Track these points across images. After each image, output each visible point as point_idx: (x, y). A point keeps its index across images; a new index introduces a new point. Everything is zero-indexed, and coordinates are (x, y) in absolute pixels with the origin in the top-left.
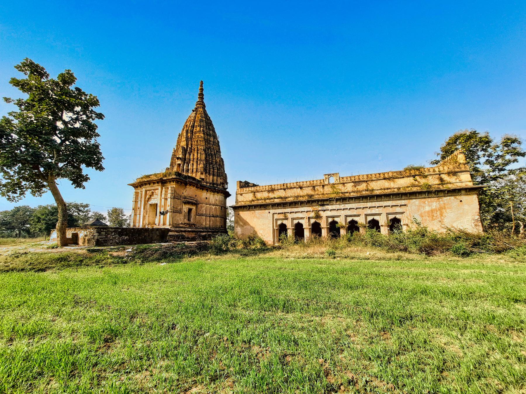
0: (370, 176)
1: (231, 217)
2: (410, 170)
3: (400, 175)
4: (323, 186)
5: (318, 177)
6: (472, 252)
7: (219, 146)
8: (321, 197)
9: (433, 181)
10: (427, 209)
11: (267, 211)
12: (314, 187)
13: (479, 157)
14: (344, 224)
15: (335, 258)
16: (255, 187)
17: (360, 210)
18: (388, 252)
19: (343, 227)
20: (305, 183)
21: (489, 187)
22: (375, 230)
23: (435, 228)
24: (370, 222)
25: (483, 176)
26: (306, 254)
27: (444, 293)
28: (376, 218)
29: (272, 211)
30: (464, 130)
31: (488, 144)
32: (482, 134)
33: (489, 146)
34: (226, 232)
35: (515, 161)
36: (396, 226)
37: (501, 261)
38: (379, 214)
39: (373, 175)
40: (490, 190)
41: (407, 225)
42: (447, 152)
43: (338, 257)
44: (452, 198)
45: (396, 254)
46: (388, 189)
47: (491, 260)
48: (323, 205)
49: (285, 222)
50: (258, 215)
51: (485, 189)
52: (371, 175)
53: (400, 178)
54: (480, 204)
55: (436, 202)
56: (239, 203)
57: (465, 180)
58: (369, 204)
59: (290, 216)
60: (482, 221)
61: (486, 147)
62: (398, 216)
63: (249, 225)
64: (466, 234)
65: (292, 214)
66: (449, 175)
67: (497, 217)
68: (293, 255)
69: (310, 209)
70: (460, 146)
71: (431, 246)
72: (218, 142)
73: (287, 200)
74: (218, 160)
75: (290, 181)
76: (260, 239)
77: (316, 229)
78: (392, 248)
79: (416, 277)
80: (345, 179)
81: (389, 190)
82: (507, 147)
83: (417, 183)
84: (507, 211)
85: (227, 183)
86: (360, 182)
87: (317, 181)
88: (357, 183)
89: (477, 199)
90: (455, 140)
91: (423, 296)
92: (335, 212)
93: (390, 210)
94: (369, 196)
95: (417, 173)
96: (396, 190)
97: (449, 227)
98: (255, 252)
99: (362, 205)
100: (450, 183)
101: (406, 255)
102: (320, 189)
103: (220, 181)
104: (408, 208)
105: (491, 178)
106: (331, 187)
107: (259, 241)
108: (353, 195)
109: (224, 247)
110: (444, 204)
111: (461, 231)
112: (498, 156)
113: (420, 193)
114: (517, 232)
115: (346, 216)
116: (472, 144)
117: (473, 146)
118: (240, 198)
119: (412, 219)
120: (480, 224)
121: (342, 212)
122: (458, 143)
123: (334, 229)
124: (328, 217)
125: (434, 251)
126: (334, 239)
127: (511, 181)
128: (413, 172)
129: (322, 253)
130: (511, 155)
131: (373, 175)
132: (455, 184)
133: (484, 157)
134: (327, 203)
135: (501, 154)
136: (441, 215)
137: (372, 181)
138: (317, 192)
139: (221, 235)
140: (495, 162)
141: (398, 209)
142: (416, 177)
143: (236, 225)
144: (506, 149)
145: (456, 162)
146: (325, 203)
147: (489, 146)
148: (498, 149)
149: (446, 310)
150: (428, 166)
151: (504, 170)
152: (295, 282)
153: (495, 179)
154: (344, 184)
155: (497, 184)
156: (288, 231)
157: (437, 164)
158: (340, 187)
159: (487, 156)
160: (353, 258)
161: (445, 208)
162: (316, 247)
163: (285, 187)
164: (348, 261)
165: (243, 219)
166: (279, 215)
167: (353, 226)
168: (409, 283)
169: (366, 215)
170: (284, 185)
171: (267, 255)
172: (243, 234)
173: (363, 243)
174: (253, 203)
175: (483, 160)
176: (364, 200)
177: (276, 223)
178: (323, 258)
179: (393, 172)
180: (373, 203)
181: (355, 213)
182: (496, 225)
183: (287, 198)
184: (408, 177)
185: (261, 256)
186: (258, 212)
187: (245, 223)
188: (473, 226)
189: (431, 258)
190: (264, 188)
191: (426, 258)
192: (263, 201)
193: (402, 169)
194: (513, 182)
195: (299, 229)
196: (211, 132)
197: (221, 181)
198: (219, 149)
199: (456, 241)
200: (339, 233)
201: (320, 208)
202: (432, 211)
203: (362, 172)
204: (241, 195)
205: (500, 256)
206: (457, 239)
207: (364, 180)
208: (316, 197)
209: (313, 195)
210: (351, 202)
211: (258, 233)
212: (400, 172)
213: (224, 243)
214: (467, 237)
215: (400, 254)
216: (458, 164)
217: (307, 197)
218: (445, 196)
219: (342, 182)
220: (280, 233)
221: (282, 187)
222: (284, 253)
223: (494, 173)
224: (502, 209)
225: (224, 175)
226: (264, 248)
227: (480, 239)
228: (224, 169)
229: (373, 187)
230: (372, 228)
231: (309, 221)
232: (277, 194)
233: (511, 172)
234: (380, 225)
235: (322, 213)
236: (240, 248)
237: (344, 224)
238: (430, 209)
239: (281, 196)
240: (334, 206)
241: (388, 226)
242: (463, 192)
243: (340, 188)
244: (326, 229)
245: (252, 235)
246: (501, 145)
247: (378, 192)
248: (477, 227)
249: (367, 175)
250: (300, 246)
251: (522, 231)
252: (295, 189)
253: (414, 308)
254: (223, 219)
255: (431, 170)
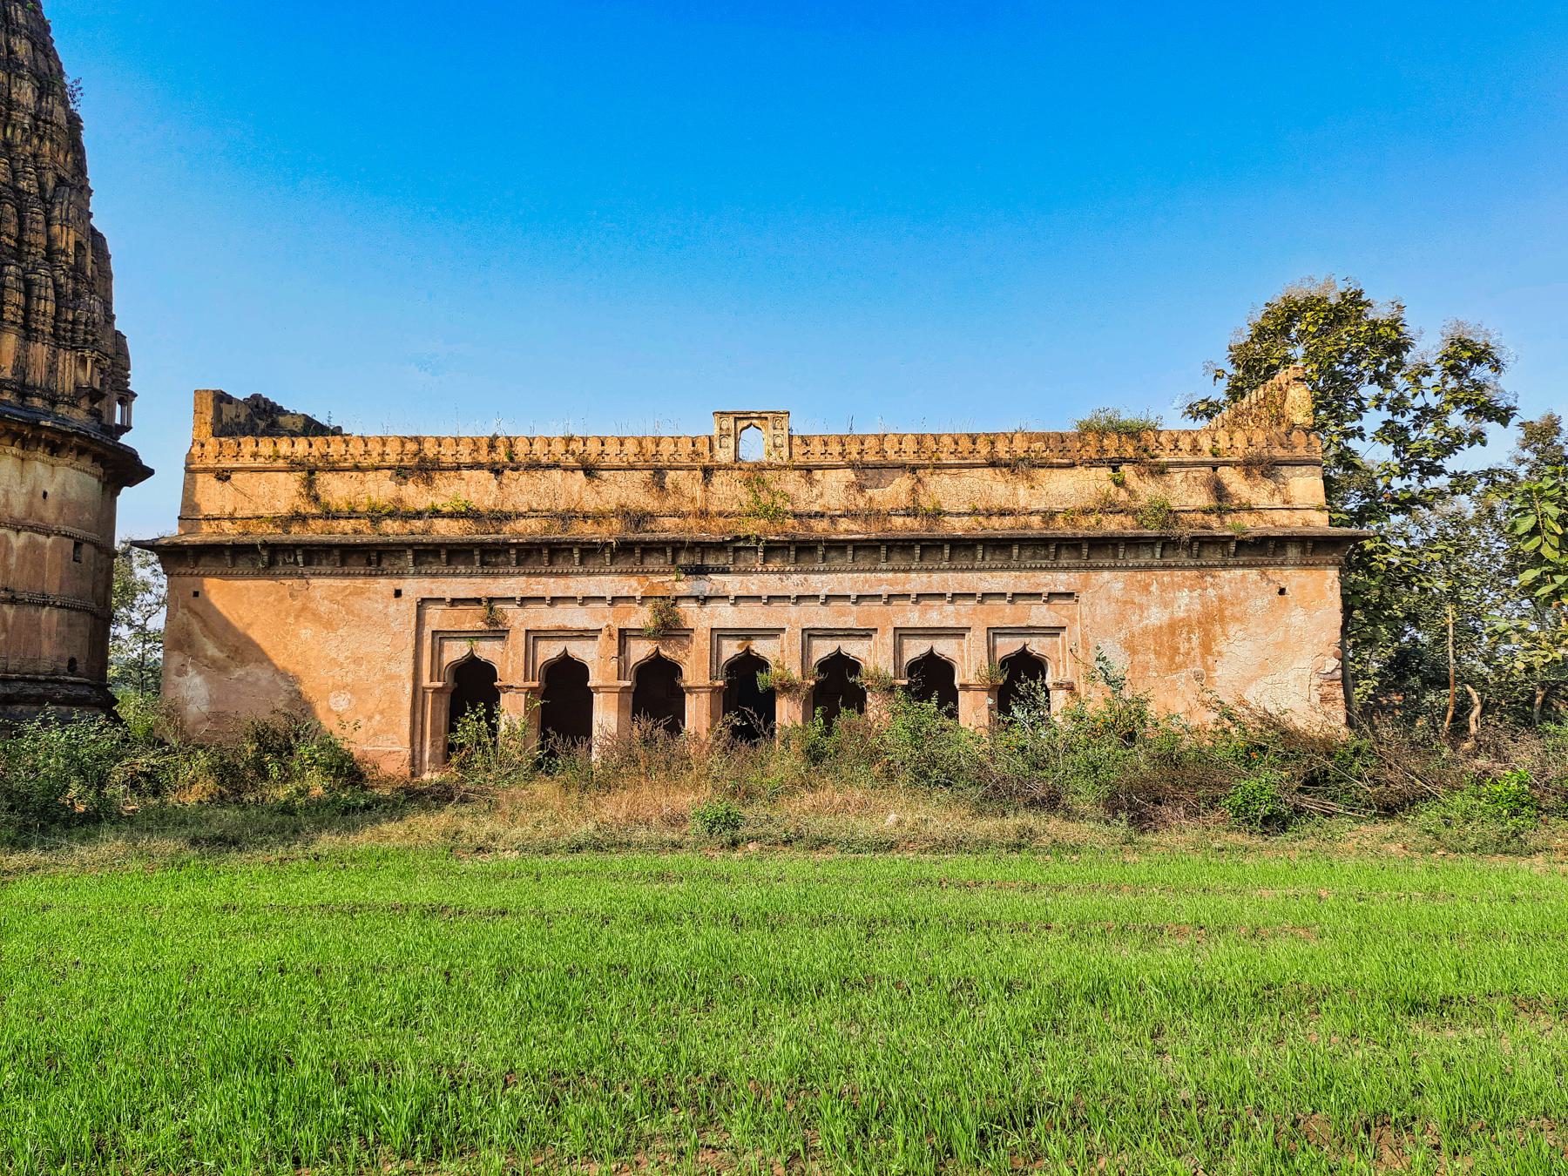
0: (930, 443)
1: (146, 611)
2: (1102, 433)
3: (1058, 453)
4: (708, 472)
5: (684, 421)
6: (1298, 811)
7: (77, 148)
8: (693, 530)
9: (1186, 494)
10: (1156, 616)
11: (384, 585)
12: (659, 472)
13: (1362, 408)
14: (796, 673)
15: (734, 844)
16: (318, 442)
17: (876, 606)
18: (981, 813)
19: (788, 688)
20: (612, 448)
21: (1384, 539)
22: (932, 706)
23: (1177, 705)
24: (914, 666)
25: (1370, 492)
26: (591, 826)
27: (1172, 995)
28: (945, 648)
29: (415, 587)
30: (1320, 279)
31: (1398, 354)
32: (1380, 312)
33: (1399, 366)
34: (107, 704)
35: (1478, 438)
36: (1022, 689)
37: (1393, 848)
38: (958, 633)
39: (947, 441)
40: (1386, 551)
41: (1071, 688)
42: (1253, 368)
43: (750, 839)
44: (1253, 574)
45: (1012, 822)
46: (1002, 513)
47: (1360, 837)
48: (700, 571)
49: (487, 651)
50: (324, 607)
51: (1369, 546)
52: (937, 439)
53: (1060, 466)
54: (1347, 610)
55: (1191, 589)
56: (206, 528)
57: (1301, 500)
58: (917, 582)
59: (519, 619)
60: (1348, 680)
61: (1388, 365)
62: (1036, 646)
63: (262, 658)
64: (1288, 735)
65: (532, 609)
66: (1248, 475)
67: (1402, 665)
68: (517, 832)
69: (630, 585)
70: (1299, 351)
71: (1157, 784)
72: (74, 122)
73: (508, 531)
74: (67, 239)
75: (537, 423)
76: (329, 746)
77: (656, 691)
78: (997, 795)
79: (1079, 930)
80: (817, 447)
81: (1008, 521)
82: (1458, 377)
83: (1123, 495)
84: (1436, 642)
85: (126, 398)
86: (885, 468)
87: (676, 440)
88: (869, 470)
89: (1337, 585)
90: (1283, 321)
91: (1094, 1014)
92: (757, 607)
93: (1006, 615)
94: (918, 541)
95: (1130, 451)
96: (1036, 520)
97: (1228, 701)
98: (289, 823)
99: (884, 581)
100: (1250, 509)
101: (1051, 826)
102: (689, 483)
103: (72, 373)
104: (1082, 609)
105: (1394, 501)
106: (748, 483)
107: (324, 757)
108: (847, 529)
109: (77, 797)
110: (1221, 599)
111: (1268, 721)
112: (1426, 411)
113: (1135, 543)
114: (1459, 729)
115: (810, 634)
116: (1341, 343)
117: (1346, 357)
118: (214, 498)
119: (1091, 661)
120: (1340, 693)
121: (793, 611)
122: (1293, 333)
123: (745, 691)
124: (719, 634)
125: (1165, 810)
126: (744, 746)
127: (1457, 521)
128: (1111, 443)
129: (676, 820)
130: (1466, 412)
131: (947, 441)
132: (1268, 515)
133: (1378, 407)
134: (722, 561)
135: (1434, 402)
136: (1206, 648)
137: (939, 467)
138: (671, 502)
139: (64, 721)
140: (1413, 435)
141: (1039, 614)
142: (1123, 468)
143: (177, 659)
144: (1452, 383)
145: (1279, 419)
146: (710, 561)
147: (1399, 366)
148: (1426, 381)
149: (1174, 1066)
150: (1174, 421)
151: (1439, 471)
152: (503, 979)
153: (1405, 505)
154: (809, 470)
155: (1412, 530)
156: (505, 700)
157: (1210, 416)
158: (792, 483)
159: (1390, 408)
160: (820, 844)
161: (1222, 619)
162: (646, 790)
163: (501, 455)
164: (795, 863)
165: (227, 625)
166: (456, 612)
167: (837, 685)
168: (1050, 958)
169: (902, 634)
170: (492, 447)
171: (364, 840)
172: (217, 717)
173: (877, 768)
174: (297, 533)
175: (1373, 420)
176: (898, 560)
177: (437, 653)
178: (676, 846)
179: (1031, 437)
180: (936, 577)
181: (850, 622)
182: (1397, 699)
183: (507, 517)
184: (1092, 464)
185: (326, 842)
186: (324, 588)
187: (242, 649)
188: (1316, 699)
189: (1149, 838)
190: (376, 449)
191: (1130, 841)
192: (364, 525)
193: (1069, 428)
194: (1465, 527)
195: (563, 694)
196: (22, 47)
197: (84, 377)
198: (80, 168)
199: (1248, 763)
200: (771, 715)
201: (685, 586)
202: (1173, 627)
203: (892, 419)
204: (223, 476)
205: (1388, 829)
206: (1253, 752)
207: (905, 458)
208: (669, 528)
209: (652, 516)
210: (838, 562)
211: (320, 710)
212: (1062, 438)
213: (81, 772)
214: (1275, 742)
215: (1030, 819)
216: (1283, 429)
217: (616, 524)
218: (1225, 566)
219: (799, 459)
220: (455, 713)
221: (483, 457)
222: (466, 825)
223: (1406, 481)
224: (1420, 636)
225: (107, 344)
226: (355, 794)
227: (1330, 755)
228: (107, 304)
229: (939, 497)
230: (923, 695)
231: (622, 648)
232: (449, 492)
233: (1462, 483)
234: (957, 682)
235: (690, 613)
236: (191, 800)
237: (796, 673)
238: (1165, 618)
239: (474, 505)
240: (754, 578)
241: (990, 690)
242: (1293, 553)
243: (790, 488)
244: (705, 697)
245: (280, 724)
246: (1439, 367)
247: (957, 527)
248: (1327, 707)
249: (920, 440)
250: (566, 787)
251: (1473, 729)
252: (557, 475)
253: (1054, 1072)
254: (83, 623)
255: (1185, 444)
